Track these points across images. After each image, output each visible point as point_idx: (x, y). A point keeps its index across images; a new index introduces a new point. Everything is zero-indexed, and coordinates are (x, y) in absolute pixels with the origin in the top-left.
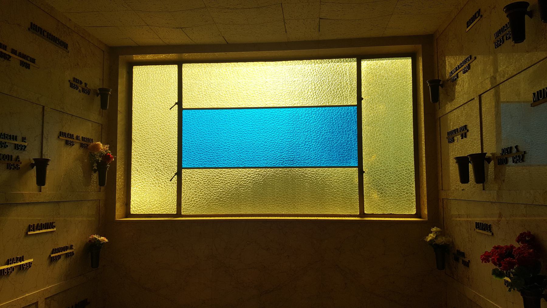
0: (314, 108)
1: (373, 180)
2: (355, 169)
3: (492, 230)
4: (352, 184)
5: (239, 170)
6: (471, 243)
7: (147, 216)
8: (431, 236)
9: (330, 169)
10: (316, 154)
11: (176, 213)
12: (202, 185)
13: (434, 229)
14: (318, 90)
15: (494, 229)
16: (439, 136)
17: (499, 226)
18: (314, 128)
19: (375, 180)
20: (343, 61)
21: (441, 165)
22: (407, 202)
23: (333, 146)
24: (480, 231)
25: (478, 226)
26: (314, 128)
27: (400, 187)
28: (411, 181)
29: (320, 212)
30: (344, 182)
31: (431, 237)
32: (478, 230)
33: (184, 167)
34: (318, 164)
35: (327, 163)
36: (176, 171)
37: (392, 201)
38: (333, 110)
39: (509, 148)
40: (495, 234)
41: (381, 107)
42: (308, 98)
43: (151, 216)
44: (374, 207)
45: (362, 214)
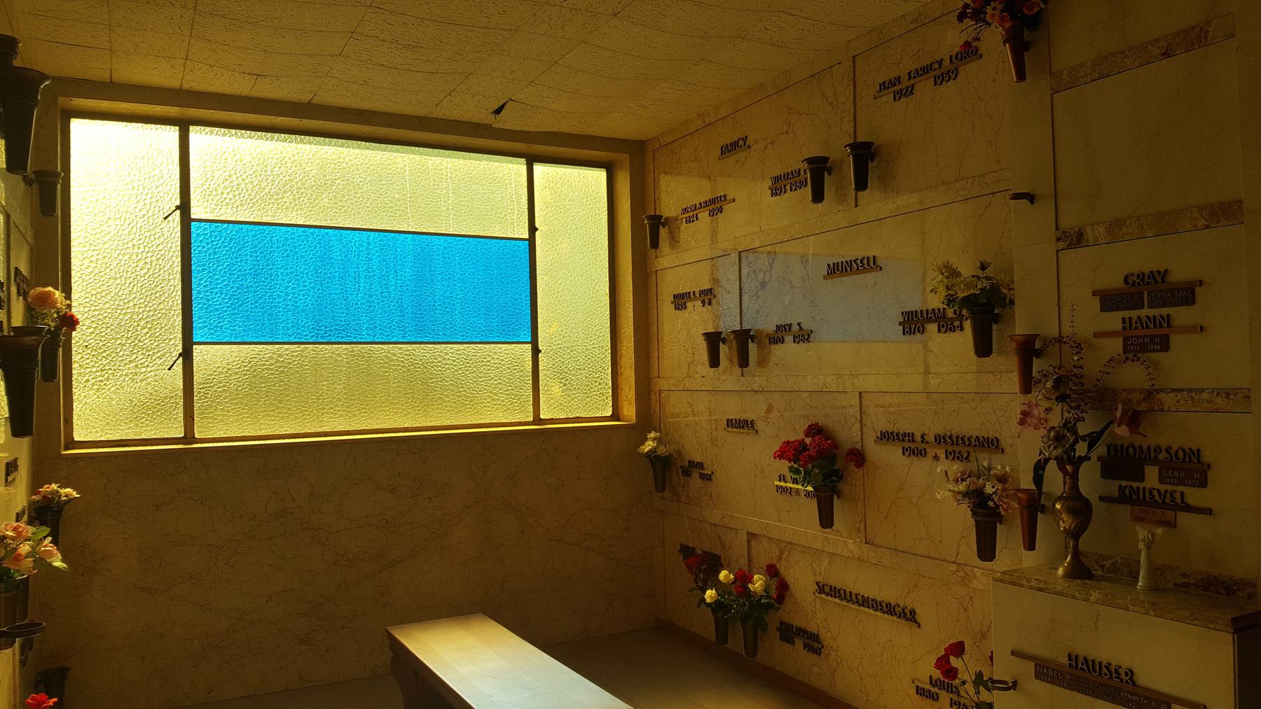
0: (217, 224)
1: (554, 365)
2: (527, 345)
3: (755, 426)
4: (522, 371)
5: (374, 348)
7: (111, 444)
8: (649, 445)
9: (487, 346)
10: (463, 320)
11: (183, 435)
12: (463, 373)
13: (652, 435)
14: (245, 191)
15: (759, 425)
16: (655, 299)
17: (768, 420)
18: (215, 266)
19: (556, 364)
20: (236, 134)
22: (600, 397)
23: (256, 302)
24: (735, 430)
25: (730, 423)
26: (215, 266)
27: (590, 375)
29: (420, 423)
30: (298, 372)
31: (649, 446)
32: (730, 429)
33: (197, 340)
34: (467, 337)
35: (330, 335)
36: (180, 349)
37: (580, 396)
38: (256, 231)
40: (760, 432)
41: (565, 245)
42: (224, 203)
43: (126, 443)
44: (555, 408)
45: (537, 420)
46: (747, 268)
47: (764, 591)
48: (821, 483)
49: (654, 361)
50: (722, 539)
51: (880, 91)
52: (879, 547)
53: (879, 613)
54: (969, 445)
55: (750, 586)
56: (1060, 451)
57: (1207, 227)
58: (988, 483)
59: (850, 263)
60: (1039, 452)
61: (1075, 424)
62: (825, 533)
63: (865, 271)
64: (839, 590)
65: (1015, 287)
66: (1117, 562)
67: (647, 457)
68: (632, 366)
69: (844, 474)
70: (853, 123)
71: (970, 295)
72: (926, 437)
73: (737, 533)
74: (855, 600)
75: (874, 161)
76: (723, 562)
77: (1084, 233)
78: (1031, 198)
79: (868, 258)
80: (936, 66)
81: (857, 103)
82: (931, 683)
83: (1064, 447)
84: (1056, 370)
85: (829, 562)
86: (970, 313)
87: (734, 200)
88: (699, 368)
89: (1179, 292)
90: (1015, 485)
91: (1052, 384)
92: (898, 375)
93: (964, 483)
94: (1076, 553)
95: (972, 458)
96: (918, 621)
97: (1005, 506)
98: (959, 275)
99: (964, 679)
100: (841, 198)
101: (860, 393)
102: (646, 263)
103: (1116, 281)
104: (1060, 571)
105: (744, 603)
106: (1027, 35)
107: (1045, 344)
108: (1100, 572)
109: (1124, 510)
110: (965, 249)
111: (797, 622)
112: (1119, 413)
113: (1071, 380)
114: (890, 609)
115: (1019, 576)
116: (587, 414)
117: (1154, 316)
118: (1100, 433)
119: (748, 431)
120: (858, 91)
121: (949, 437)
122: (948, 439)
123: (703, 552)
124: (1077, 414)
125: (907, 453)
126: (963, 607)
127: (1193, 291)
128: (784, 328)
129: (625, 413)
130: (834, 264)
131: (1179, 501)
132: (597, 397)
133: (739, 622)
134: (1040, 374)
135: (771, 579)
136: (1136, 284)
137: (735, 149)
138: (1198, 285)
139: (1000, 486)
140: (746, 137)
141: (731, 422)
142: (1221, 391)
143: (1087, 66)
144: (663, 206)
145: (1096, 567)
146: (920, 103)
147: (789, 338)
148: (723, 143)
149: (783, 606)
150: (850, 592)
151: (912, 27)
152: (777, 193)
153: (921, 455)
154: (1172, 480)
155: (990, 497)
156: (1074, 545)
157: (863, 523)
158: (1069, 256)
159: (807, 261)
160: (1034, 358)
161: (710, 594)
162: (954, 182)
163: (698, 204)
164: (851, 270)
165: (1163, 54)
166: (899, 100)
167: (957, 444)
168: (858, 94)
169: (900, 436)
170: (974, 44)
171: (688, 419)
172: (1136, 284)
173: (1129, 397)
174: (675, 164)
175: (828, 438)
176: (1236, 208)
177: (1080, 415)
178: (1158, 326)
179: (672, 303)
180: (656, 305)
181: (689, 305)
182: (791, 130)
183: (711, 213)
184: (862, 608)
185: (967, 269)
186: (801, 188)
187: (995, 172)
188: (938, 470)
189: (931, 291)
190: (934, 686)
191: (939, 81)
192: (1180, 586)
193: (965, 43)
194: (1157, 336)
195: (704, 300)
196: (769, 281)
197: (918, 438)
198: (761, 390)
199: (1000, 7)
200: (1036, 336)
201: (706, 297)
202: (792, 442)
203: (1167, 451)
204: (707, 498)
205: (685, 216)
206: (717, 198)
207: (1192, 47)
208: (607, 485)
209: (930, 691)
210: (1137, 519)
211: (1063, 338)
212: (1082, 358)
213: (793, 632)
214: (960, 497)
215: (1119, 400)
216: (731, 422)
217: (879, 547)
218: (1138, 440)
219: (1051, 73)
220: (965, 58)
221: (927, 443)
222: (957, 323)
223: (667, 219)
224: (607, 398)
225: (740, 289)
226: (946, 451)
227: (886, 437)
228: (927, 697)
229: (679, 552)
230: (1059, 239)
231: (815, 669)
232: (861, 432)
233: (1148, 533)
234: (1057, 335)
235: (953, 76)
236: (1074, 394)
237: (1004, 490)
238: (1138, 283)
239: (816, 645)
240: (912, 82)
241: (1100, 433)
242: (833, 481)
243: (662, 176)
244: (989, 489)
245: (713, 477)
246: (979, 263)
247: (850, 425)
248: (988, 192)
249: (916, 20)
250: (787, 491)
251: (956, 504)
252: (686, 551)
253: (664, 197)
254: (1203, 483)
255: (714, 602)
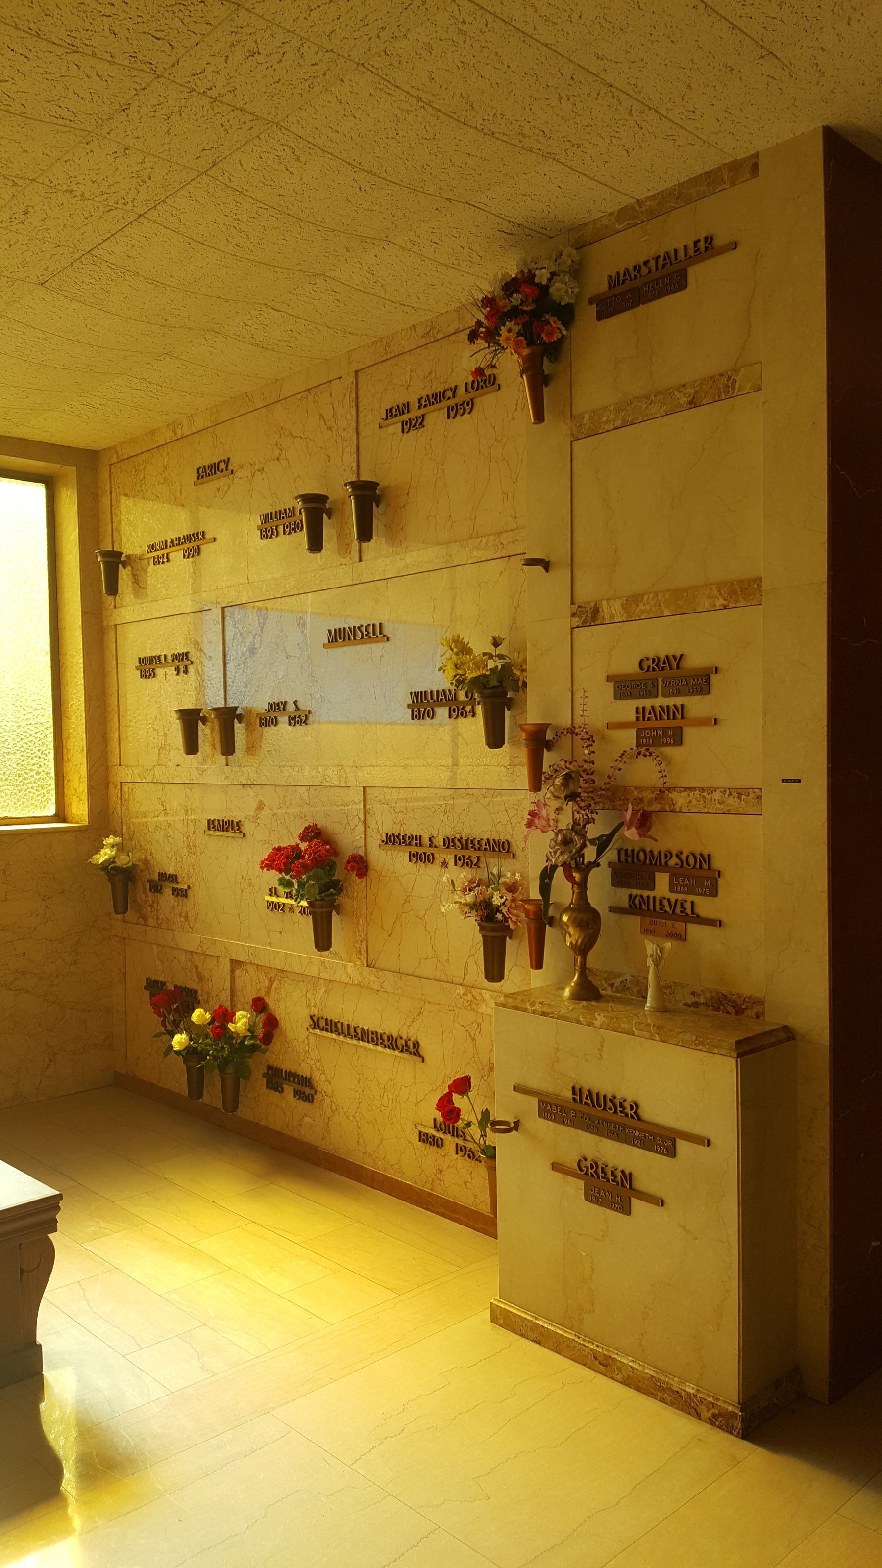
3: (242, 829)
6: (194, 856)
13: (111, 840)
15: (247, 827)
16: (115, 662)
21: (119, 718)
22: (37, 790)
24: (217, 833)
25: (212, 825)
27: (23, 761)
28: (45, 748)
32: (211, 832)
39: (282, 702)
40: (247, 835)
46: (233, 629)
47: (249, 1030)
48: (317, 897)
49: (114, 744)
50: (199, 970)
51: (387, 419)
52: (381, 970)
53: (379, 1048)
54: (479, 849)
55: (231, 1026)
56: (566, 857)
57: (725, 607)
58: (495, 893)
59: (353, 630)
60: (546, 859)
61: (584, 826)
62: (322, 956)
63: (371, 640)
64: (335, 1023)
65: (528, 668)
66: (626, 980)
67: (102, 869)
68: (83, 750)
69: (345, 885)
70: (355, 455)
71: (479, 676)
72: (434, 840)
73: (218, 962)
74: (353, 1034)
75: (381, 506)
76: (200, 998)
77: (600, 610)
78: (546, 565)
79: (373, 625)
80: (449, 394)
81: (360, 430)
82: (435, 1127)
83: (571, 852)
84: (568, 765)
85: (326, 991)
86: (481, 697)
87: (215, 540)
88: (172, 755)
89: (694, 680)
90: (525, 896)
91: (561, 781)
92: (405, 767)
93: (472, 893)
94: (584, 970)
95: (482, 865)
96: (422, 1054)
97: (514, 919)
98: (469, 651)
99: (470, 1119)
100: (344, 549)
101: (364, 788)
102: (101, 614)
103: (630, 666)
104: (567, 992)
105: (223, 1047)
106: (547, 367)
107: (556, 735)
108: (609, 992)
109: (634, 922)
110: (477, 621)
111: (287, 1064)
112: (628, 815)
113: (581, 777)
114: (391, 1042)
115: (523, 1000)
116: (19, 813)
117: (668, 706)
118: (610, 837)
119: (233, 835)
120: (361, 415)
121: (458, 840)
122: (457, 843)
123: (176, 987)
124: (586, 815)
125: (414, 859)
126: (470, 1035)
127: (708, 681)
128: (278, 707)
129: (74, 811)
130: (335, 630)
131: (689, 911)
132: (33, 791)
133: (217, 1071)
134: (552, 768)
135: (257, 1016)
136: (651, 669)
137: (215, 473)
138: (714, 672)
139: (509, 896)
140: (229, 459)
141: (213, 824)
142: (733, 790)
143: (611, 410)
144: (124, 540)
145: (605, 985)
146: (431, 439)
147: (283, 719)
148: (200, 463)
149: (270, 1047)
150: (349, 1025)
151: (423, 341)
152: (159, 562)
153: (429, 862)
154: (682, 888)
155: (498, 910)
156: (581, 962)
157: (364, 943)
158: (583, 634)
159: (304, 625)
160: (545, 751)
161: (179, 1040)
162: (467, 540)
163: (169, 540)
164: (355, 639)
165: (690, 403)
166: (408, 432)
167: (467, 848)
168: (361, 420)
169: (407, 839)
170: (488, 372)
171: (159, 819)
172: (651, 669)
173: (640, 796)
174: (138, 485)
175: (327, 843)
176: (755, 586)
177: (590, 815)
178: (672, 717)
179: (137, 668)
180: (115, 671)
181: (160, 672)
182: (283, 456)
183: (187, 554)
184: (361, 1042)
185: (479, 645)
186: (295, 532)
187: (512, 530)
188: (445, 879)
189: (440, 669)
190: (438, 1131)
191: (452, 414)
192: (689, 1006)
193: (476, 369)
194: (670, 728)
195: (178, 667)
196: (260, 647)
197: (426, 841)
198: (250, 783)
199: (516, 329)
200: (547, 726)
201: (181, 663)
202: (284, 848)
203: (677, 856)
204: (182, 919)
205: (151, 555)
206: (193, 535)
207: (719, 396)
208: (47, 906)
209: (434, 1137)
210: (647, 931)
211: (574, 727)
212: (594, 752)
213: (282, 1076)
214: (467, 909)
215: (631, 800)
216: (213, 824)
217: (381, 970)
218: (649, 845)
219: (571, 416)
220: (482, 387)
221: (435, 847)
222: (469, 708)
223: (129, 557)
224: (48, 792)
225: (225, 655)
226: (456, 856)
227: (392, 840)
228: (431, 1144)
229: (145, 988)
230: (574, 615)
231: (307, 1119)
232: (365, 835)
233: (656, 948)
234: (569, 725)
235: (468, 409)
236: (585, 792)
237: (514, 900)
238: (653, 668)
239: (308, 1091)
240: (470, 396)
241: (610, 837)
242: (332, 894)
243: (123, 499)
244: (497, 901)
245: (190, 893)
246: (492, 638)
247: (352, 827)
248: (503, 555)
249: (427, 333)
250: (279, 908)
251: (462, 917)
252: (153, 986)
253: (125, 528)
254: (713, 892)
255: (184, 1050)
